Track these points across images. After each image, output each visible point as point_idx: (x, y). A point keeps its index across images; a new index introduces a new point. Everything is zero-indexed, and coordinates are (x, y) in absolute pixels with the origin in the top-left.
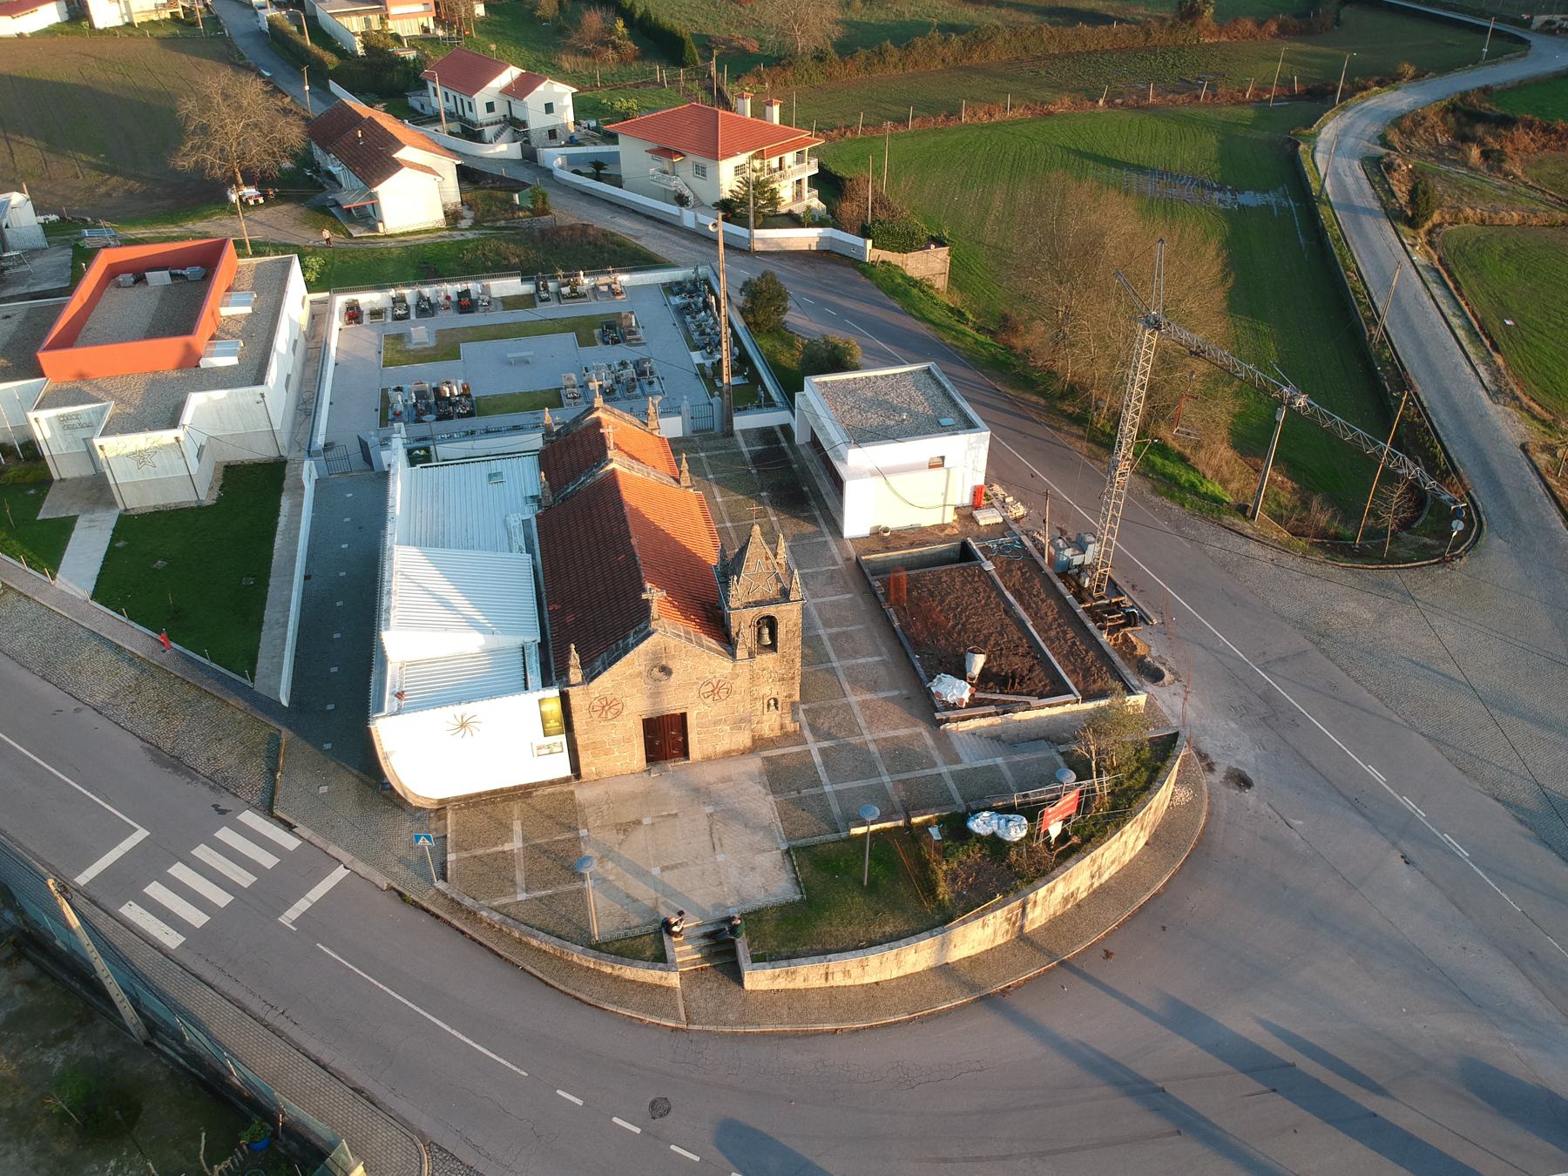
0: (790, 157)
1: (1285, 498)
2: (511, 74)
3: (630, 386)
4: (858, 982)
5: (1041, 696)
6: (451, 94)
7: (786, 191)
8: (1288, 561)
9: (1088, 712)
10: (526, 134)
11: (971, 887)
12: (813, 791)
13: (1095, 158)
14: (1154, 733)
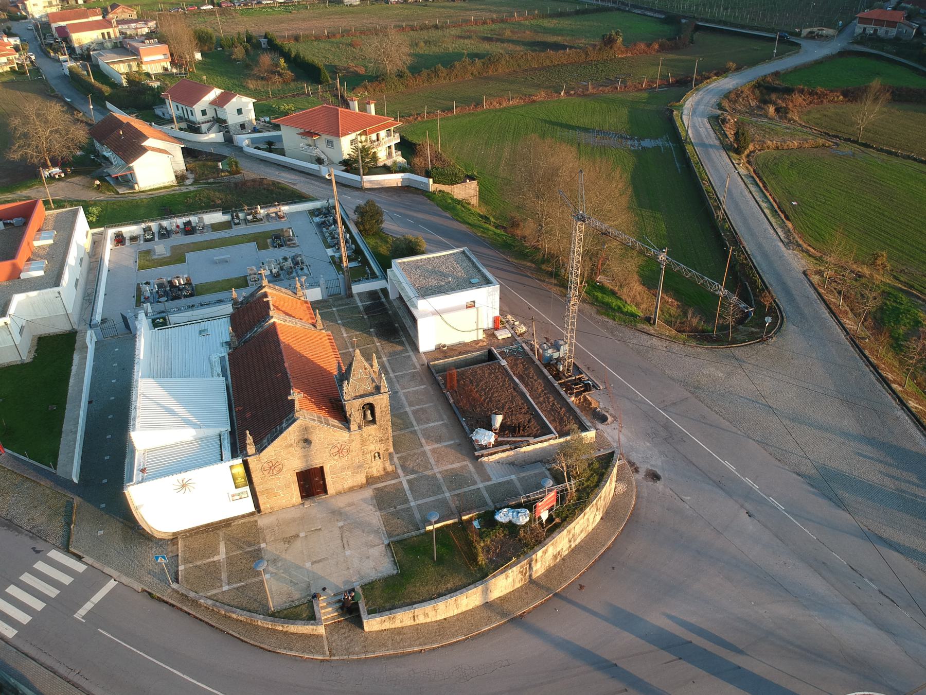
0: (383, 134)
1: (673, 311)
2: (215, 93)
3: (290, 272)
4: (433, 620)
5: (535, 437)
6: (180, 106)
7: (382, 155)
8: (676, 347)
9: (561, 444)
10: (227, 127)
11: (498, 555)
12: (403, 506)
13: (561, 125)
14: (603, 452)
